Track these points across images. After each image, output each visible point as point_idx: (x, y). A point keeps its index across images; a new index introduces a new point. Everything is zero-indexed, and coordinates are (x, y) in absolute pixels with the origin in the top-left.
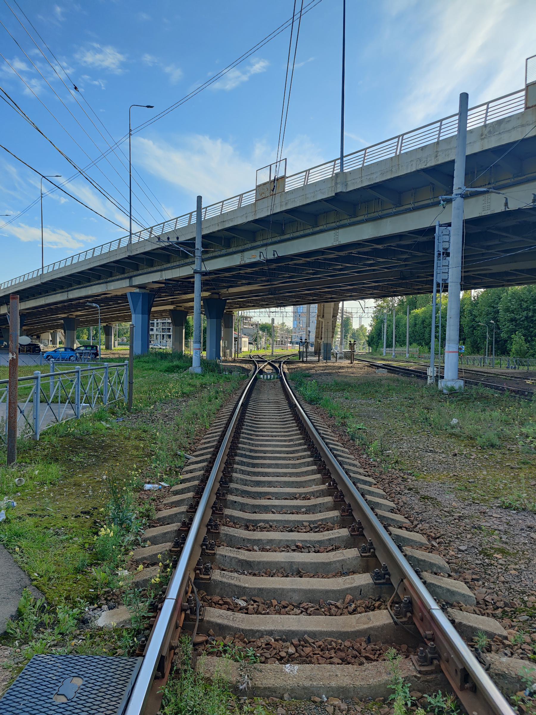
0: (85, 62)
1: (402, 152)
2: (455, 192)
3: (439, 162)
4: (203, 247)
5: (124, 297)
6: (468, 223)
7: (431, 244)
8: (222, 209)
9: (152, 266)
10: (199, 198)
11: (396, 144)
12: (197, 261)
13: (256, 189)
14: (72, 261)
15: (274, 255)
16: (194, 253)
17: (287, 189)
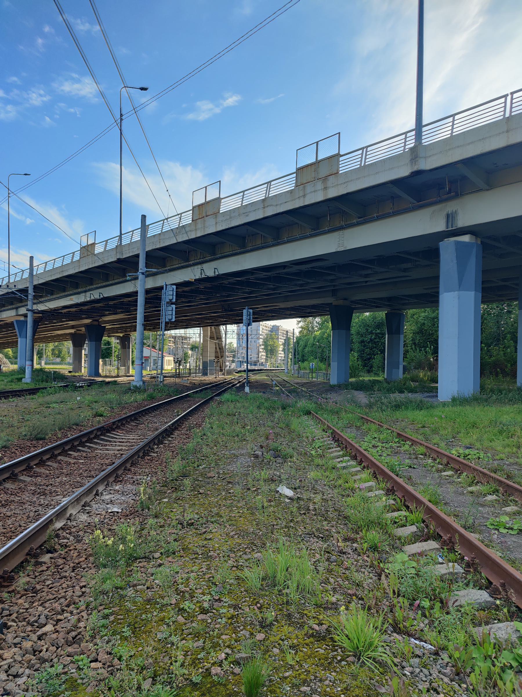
0: (62, 90)
1: (270, 196)
2: (140, 271)
3: (307, 203)
4: (34, 292)
5: (11, 325)
6: (148, 292)
8: (163, 228)
9: (107, 280)
10: (144, 217)
11: (360, 156)
12: (29, 303)
13: (80, 250)
15: (100, 296)
16: (27, 296)
17: (222, 210)
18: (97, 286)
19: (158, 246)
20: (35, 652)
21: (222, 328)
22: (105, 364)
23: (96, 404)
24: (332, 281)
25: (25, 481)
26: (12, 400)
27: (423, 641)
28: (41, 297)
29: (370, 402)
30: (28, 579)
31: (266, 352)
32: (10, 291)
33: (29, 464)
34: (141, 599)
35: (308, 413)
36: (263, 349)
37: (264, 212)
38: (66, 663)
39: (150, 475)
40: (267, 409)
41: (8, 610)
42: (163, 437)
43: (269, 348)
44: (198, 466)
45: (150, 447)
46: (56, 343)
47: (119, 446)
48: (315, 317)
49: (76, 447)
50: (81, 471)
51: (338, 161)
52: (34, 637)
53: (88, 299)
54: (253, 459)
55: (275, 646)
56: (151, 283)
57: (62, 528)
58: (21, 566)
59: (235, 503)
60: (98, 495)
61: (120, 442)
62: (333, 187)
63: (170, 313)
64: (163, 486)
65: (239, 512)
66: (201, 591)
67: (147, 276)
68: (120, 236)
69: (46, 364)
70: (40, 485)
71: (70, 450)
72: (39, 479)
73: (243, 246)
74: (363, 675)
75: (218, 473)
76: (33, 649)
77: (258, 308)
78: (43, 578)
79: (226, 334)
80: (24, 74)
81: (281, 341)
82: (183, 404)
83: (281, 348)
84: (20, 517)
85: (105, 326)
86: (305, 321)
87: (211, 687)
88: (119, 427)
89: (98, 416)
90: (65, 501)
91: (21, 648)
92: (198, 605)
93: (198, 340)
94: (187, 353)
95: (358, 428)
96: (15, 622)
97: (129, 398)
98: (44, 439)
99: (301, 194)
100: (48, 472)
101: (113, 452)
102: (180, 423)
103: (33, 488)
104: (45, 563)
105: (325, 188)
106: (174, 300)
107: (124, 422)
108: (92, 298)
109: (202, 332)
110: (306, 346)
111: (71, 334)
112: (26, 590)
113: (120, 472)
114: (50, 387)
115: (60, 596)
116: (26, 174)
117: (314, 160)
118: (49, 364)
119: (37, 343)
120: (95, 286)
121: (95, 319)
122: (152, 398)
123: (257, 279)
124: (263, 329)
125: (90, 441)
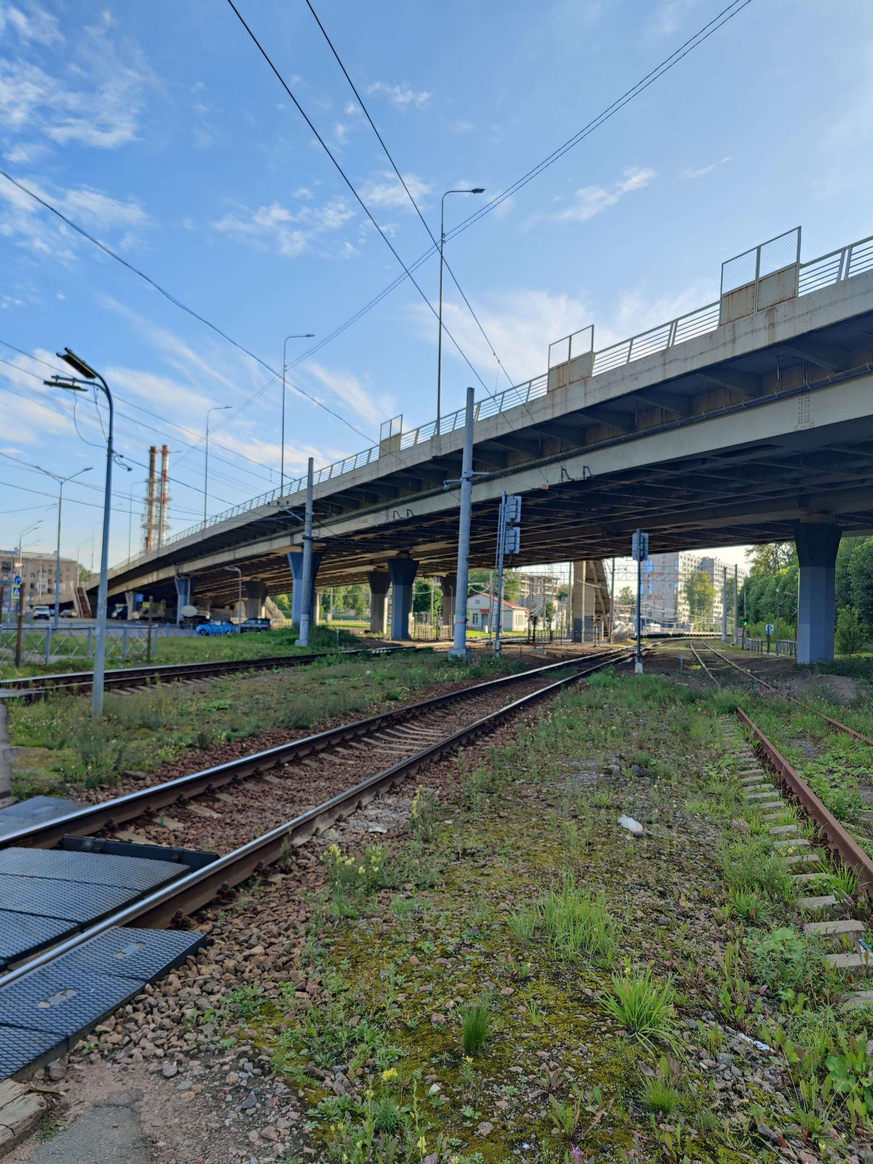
0: (371, 200)
1: (675, 344)
2: (464, 475)
4: (314, 510)
6: (475, 507)
7: (495, 516)
8: (630, 354)
9: (419, 489)
12: (307, 527)
14: (369, 457)
15: (584, 473)
16: (303, 517)
17: (595, 373)
18: (404, 499)
19: (494, 435)
20: (236, 971)
21: (607, 563)
22: (419, 619)
23: (390, 682)
24: (796, 481)
25: (271, 783)
26: (276, 671)
27: (759, 1040)
28: (325, 517)
29: (860, 696)
30: (251, 899)
31: (692, 604)
32: (282, 510)
33: (279, 760)
34: (372, 932)
35: (732, 710)
36: (684, 598)
37: (665, 371)
38: (269, 987)
39: (440, 788)
40: (661, 701)
41: (219, 928)
42: (477, 736)
43: (696, 597)
44: (514, 780)
45: (451, 748)
46: (350, 587)
47: (410, 744)
48: (780, 541)
49: (347, 741)
50: (347, 775)
51: (797, 276)
52: (240, 957)
53: (391, 520)
54: (602, 775)
55: (522, 1004)
56: (482, 493)
57: (305, 846)
58: (246, 884)
59: (545, 833)
60: (360, 808)
61: (413, 739)
62: (785, 321)
63: (512, 540)
64: (452, 804)
65: (545, 846)
66: (450, 933)
67: (474, 483)
68: (438, 422)
69: (334, 618)
70: (290, 790)
71: (338, 745)
72: (289, 782)
73: (632, 428)
74: (630, 1053)
75: (539, 791)
76: (235, 969)
77: (665, 529)
78: (268, 899)
79: (613, 574)
80: (318, 183)
81: (718, 586)
82: (526, 688)
83: (718, 597)
84: (256, 827)
85: (418, 561)
86: (761, 551)
87: (427, 1035)
88: (417, 717)
89: (391, 700)
90: (311, 811)
91: (222, 966)
92: (441, 947)
93: (567, 582)
94: (551, 605)
95: (817, 740)
96: (225, 941)
97: (443, 675)
98: (307, 728)
99: (729, 337)
100: (303, 773)
101: (398, 753)
102: (511, 716)
103: (280, 793)
104: (275, 884)
105: (772, 325)
106: (518, 520)
107: (425, 710)
108: (397, 518)
109: (573, 570)
110: (762, 594)
111: (369, 573)
112: (245, 910)
113: (398, 781)
114: (331, 655)
115: (281, 920)
116: (308, 336)
117: (752, 278)
118: (339, 618)
119: (322, 587)
120: (401, 499)
121: (403, 549)
122: (477, 675)
123: (657, 481)
124: (684, 564)
125: (369, 734)
